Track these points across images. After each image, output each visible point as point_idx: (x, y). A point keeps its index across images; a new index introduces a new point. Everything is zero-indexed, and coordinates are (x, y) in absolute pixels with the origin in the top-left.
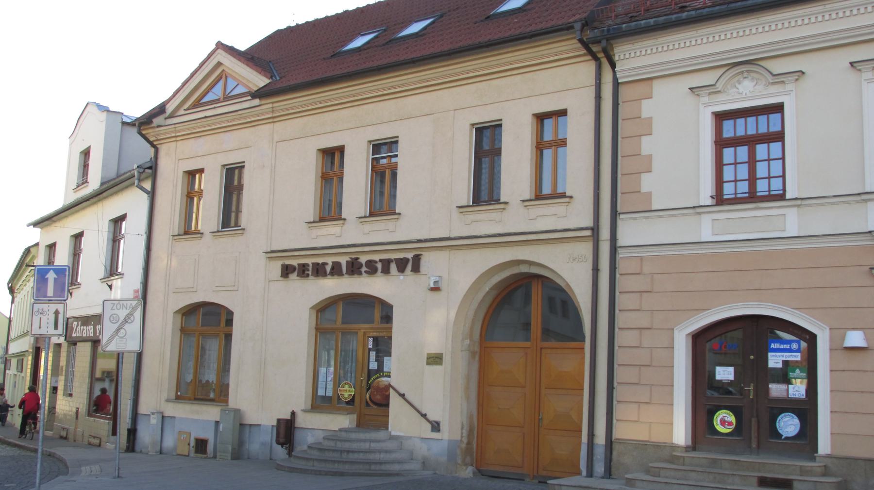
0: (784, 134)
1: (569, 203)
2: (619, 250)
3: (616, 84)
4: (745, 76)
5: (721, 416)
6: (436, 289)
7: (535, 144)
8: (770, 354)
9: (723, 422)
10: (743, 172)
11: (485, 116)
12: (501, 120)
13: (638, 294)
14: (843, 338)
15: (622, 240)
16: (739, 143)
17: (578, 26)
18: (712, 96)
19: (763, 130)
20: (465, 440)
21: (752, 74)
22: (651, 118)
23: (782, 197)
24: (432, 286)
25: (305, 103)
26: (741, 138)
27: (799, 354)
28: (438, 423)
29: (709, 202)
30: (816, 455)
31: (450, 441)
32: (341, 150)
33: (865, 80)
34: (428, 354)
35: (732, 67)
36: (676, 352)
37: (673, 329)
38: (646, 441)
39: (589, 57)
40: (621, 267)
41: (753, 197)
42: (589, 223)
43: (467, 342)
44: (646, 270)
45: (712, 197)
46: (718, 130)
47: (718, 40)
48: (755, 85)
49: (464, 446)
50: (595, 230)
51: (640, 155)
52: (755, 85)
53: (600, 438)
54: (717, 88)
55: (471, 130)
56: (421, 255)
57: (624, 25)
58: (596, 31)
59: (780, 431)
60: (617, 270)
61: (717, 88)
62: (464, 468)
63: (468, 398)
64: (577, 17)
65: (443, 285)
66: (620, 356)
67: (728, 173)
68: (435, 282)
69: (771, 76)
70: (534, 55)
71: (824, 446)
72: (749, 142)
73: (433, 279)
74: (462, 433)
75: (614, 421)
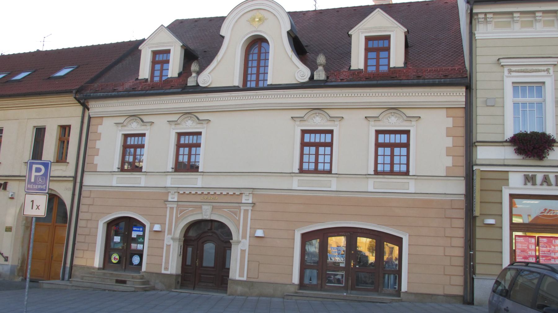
0: (333, 144)
1: (67, 165)
2: (83, 187)
3: (90, 118)
4: (317, 115)
5: (114, 256)
6: (12, 198)
7: (58, 138)
8: (133, 232)
9: (115, 259)
10: (388, 160)
11: (40, 124)
12: (3, 128)
13: (88, 206)
14: (153, 227)
15: (85, 183)
16: (197, 146)
17: (74, 91)
18: (176, 125)
19: (323, 140)
20: (20, 265)
21: (320, 115)
22: (101, 133)
23: (330, 172)
24: (10, 196)
25: (22, 102)
26: (132, 145)
27: (142, 232)
28: (7, 257)
29: (171, 170)
30: (140, 271)
31: (12, 265)
32: (69, 127)
33: (297, 125)
34: (6, 227)
35: (311, 111)
36: (99, 230)
37: (98, 221)
38: (85, 266)
39: (79, 104)
40: (83, 194)
41: (316, 171)
42: (73, 174)
43: (24, 222)
44: (92, 196)
45: (118, 168)
46: (303, 138)
47: (290, 97)
48: (193, 123)
49: (19, 267)
50: (75, 178)
51: (95, 148)
52: (193, 123)
53: (68, 265)
54: (304, 119)
55: (33, 129)
56: (7, 182)
57: (92, 94)
58: (82, 95)
59: (133, 263)
60: (82, 195)
61: (304, 119)
62: (18, 277)
63: (23, 247)
64: (75, 88)
65: (15, 197)
66: (79, 231)
67: (306, 158)
68: (12, 195)
69: (329, 117)
70: (40, 101)
71: (144, 268)
72: (189, 146)
73: (11, 194)
74: (19, 262)
75: (74, 257)
